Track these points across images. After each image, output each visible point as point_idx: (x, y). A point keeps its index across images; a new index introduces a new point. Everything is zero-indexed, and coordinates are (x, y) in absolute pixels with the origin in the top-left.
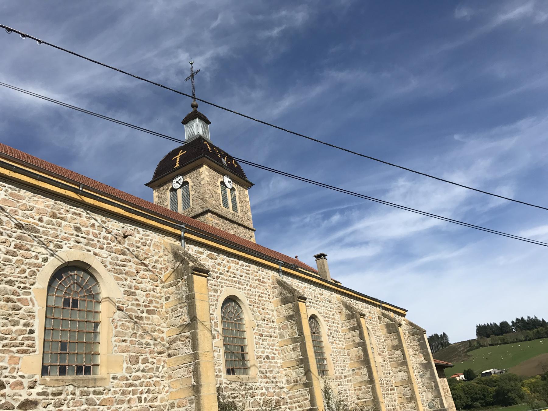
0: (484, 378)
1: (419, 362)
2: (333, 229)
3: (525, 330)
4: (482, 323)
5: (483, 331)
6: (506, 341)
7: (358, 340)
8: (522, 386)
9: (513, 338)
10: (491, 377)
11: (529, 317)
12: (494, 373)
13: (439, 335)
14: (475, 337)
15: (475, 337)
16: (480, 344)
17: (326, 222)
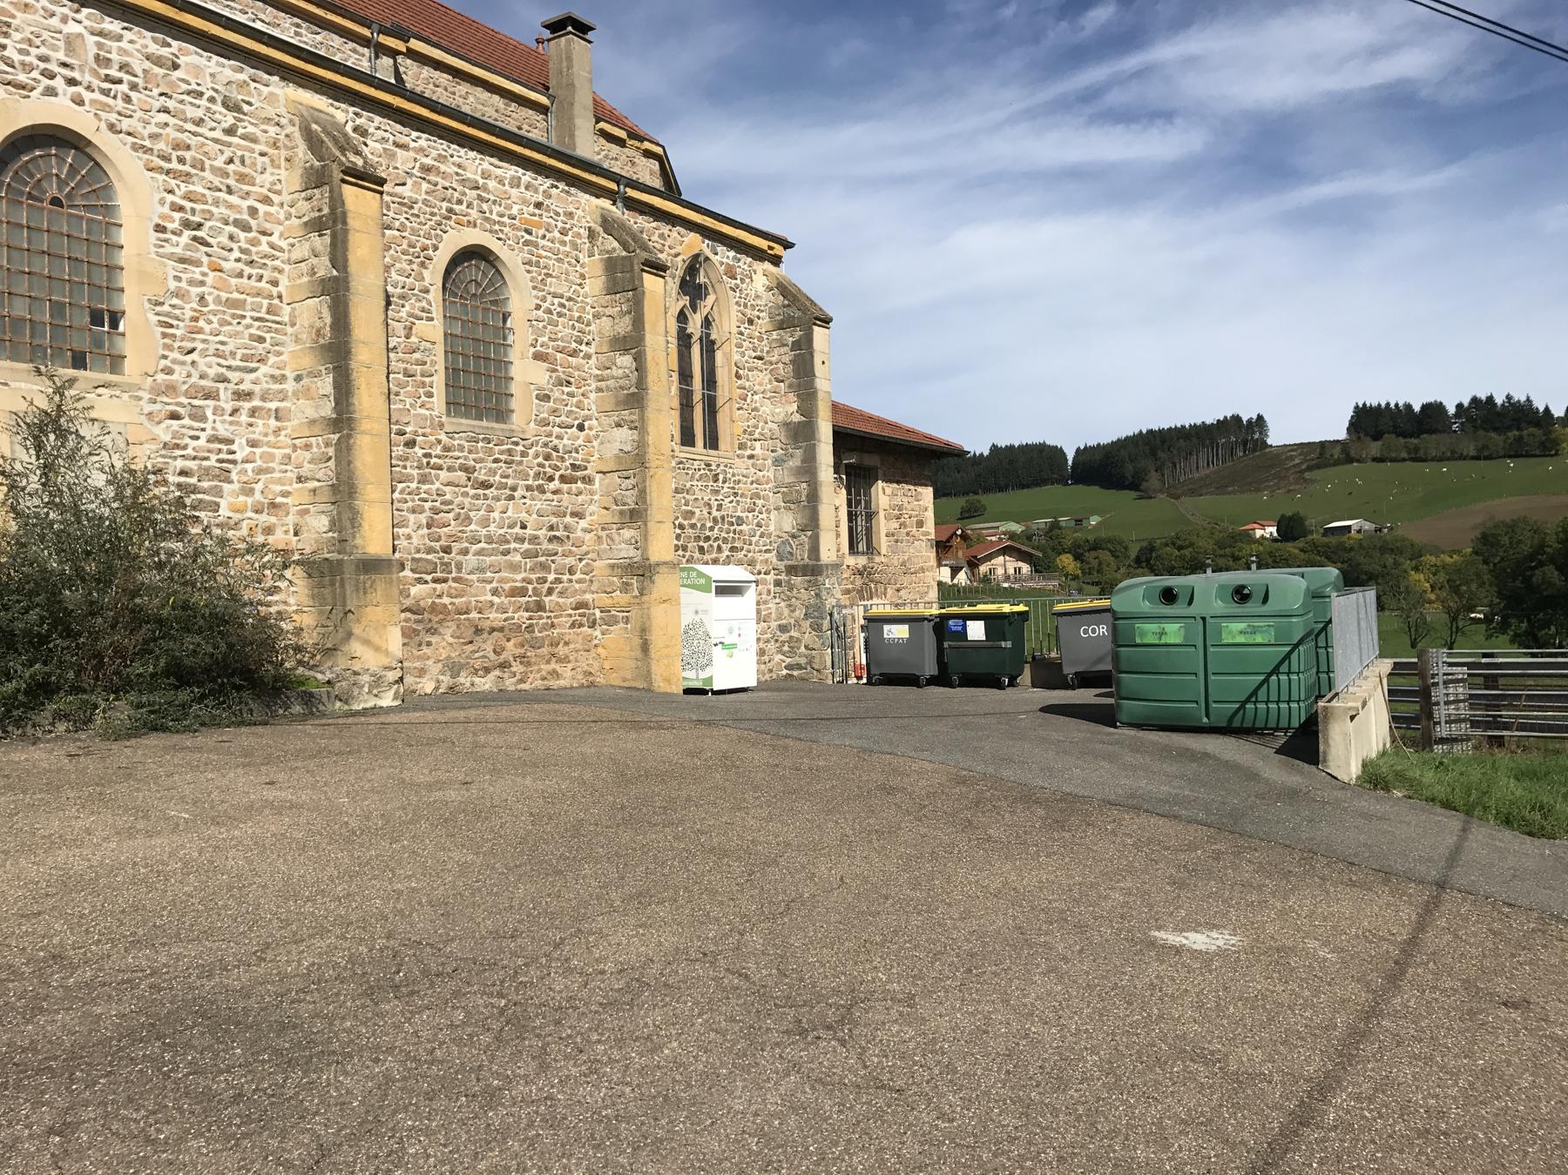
0: (1333, 540)
1: (780, 418)
2: (1078, 55)
3: (1487, 430)
4: (1372, 401)
5: (1367, 420)
6: (1421, 454)
7: (324, 268)
8: (1416, 569)
9: (1443, 449)
10: (1344, 538)
11: (1509, 397)
12: (1359, 531)
13: (1245, 419)
14: (1342, 435)
15: (1342, 435)
16: (1348, 455)
17: (1064, 24)
